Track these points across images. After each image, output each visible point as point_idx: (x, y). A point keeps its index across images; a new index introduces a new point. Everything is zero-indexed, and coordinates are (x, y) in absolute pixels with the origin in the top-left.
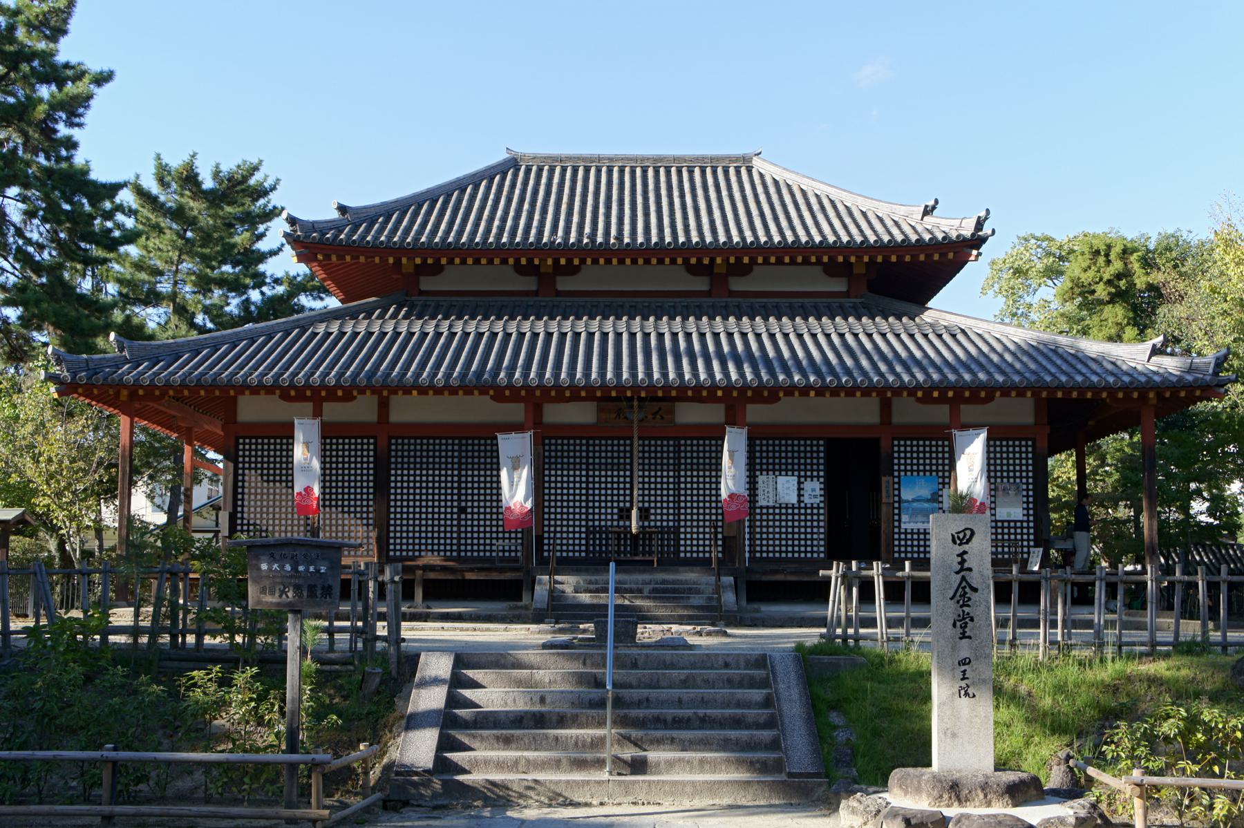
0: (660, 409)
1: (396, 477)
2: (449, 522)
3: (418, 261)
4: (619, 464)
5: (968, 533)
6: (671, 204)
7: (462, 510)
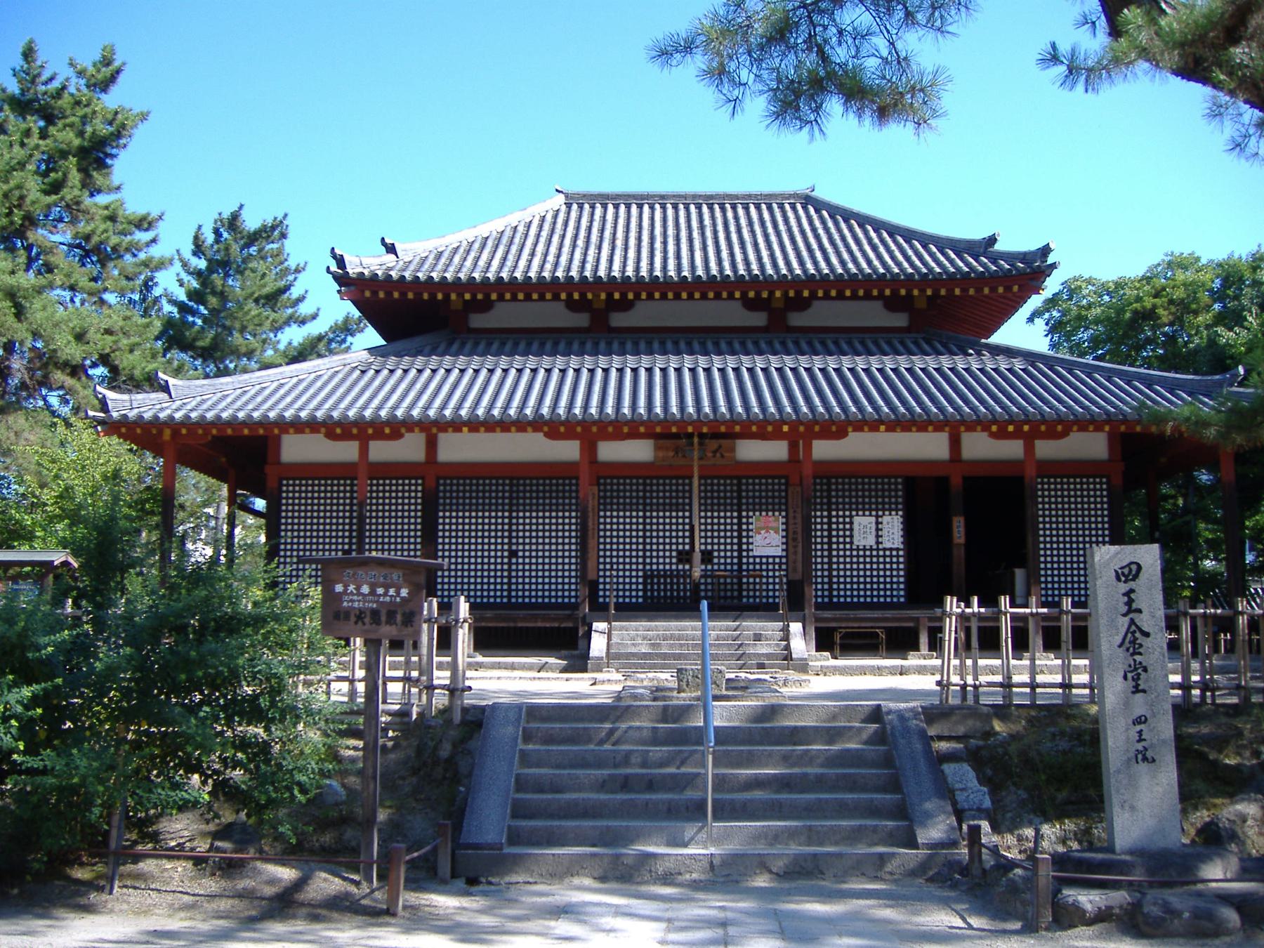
0: (720, 447)
1: (445, 519)
2: (499, 567)
3: (467, 296)
4: (677, 504)
5: (1134, 567)
6: (728, 238)
7: (513, 554)
